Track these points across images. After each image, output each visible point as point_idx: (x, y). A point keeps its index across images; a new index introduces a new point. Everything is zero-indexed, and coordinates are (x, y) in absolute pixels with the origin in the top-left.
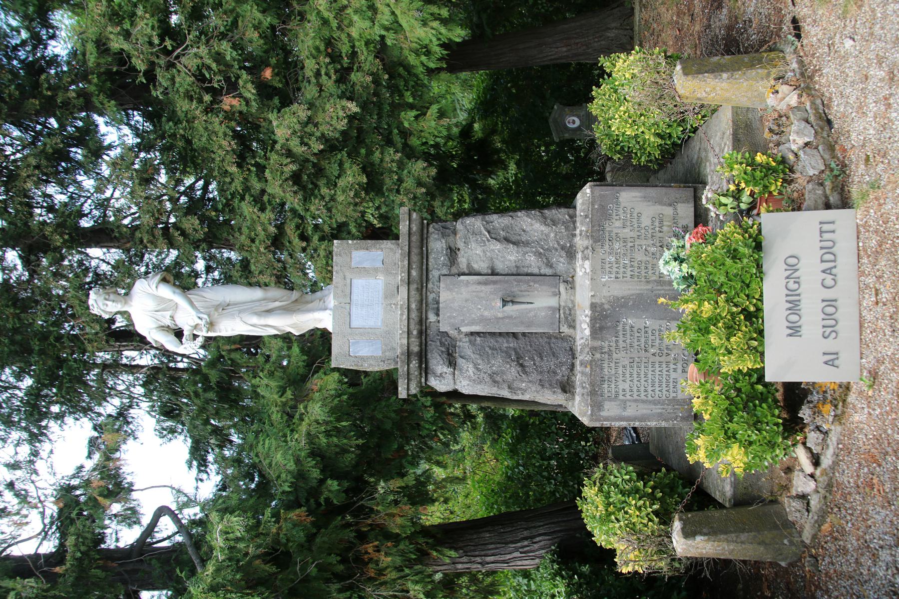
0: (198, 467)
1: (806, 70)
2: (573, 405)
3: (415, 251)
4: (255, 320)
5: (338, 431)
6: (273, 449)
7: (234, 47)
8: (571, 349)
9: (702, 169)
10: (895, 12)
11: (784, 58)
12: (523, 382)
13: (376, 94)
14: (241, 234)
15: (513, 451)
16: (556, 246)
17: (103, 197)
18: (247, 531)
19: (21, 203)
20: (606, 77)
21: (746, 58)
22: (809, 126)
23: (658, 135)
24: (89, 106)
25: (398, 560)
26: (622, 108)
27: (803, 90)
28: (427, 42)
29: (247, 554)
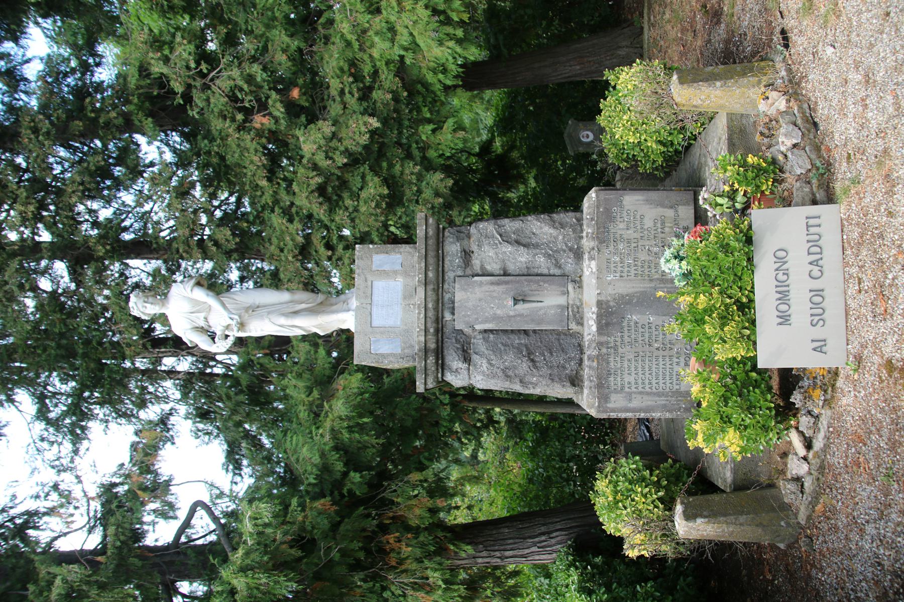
1: (794, 77)
2: (582, 400)
3: (432, 254)
4: (283, 321)
5: (362, 428)
6: (300, 445)
7: (265, 69)
8: (579, 345)
10: (868, 20)
11: (773, 66)
12: (534, 376)
13: (396, 111)
14: (271, 244)
16: (564, 247)
17: (142, 210)
19: (67, 217)
20: (611, 89)
21: (738, 67)
22: (796, 129)
23: (660, 142)
24: (129, 126)
25: (418, 552)
26: (625, 117)
28: (444, 61)
29: (275, 540)
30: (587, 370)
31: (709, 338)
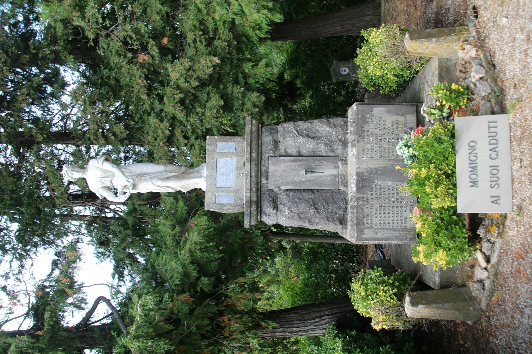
0: (118, 278)
1: (481, 36)
2: (346, 232)
3: (254, 142)
4: (160, 183)
6: (168, 261)
8: (345, 199)
9: (421, 95)
11: (468, 29)
12: (317, 218)
14: (149, 135)
15: (308, 268)
16: (336, 139)
17: (66, 113)
18: (156, 305)
20: (365, 42)
21: (446, 30)
22: (482, 68)
24: (58, 59)
25: (242, 328)
26: (374, 60)
27: (479, 47)
28: (260, 22)
30: (350, 215)
31: (428, 195)
